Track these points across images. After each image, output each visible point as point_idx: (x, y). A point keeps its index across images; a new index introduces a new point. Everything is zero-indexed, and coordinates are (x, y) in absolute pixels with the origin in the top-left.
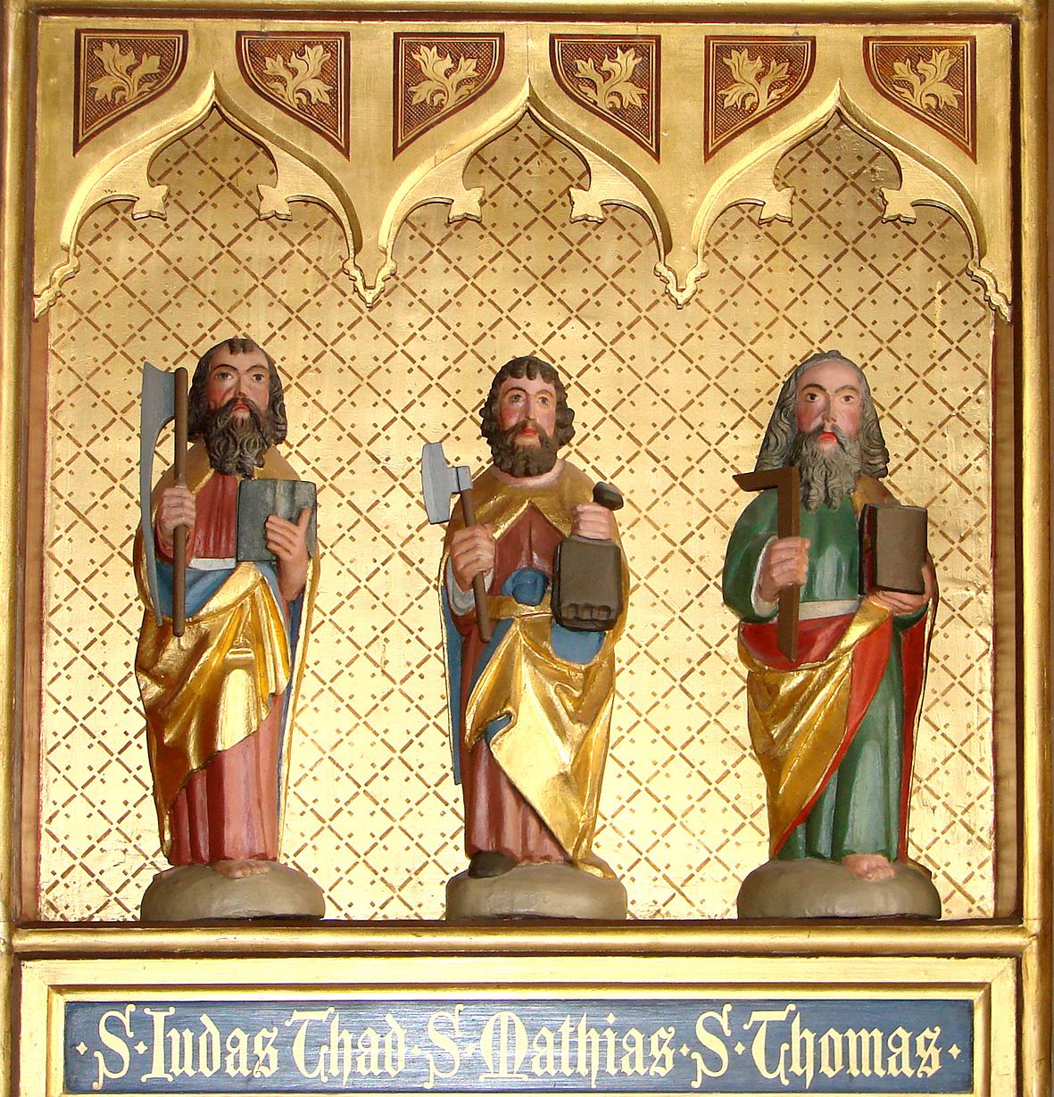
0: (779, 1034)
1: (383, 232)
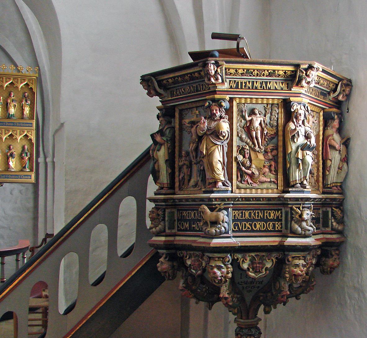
0: (23, 176)
1: (19, 139)
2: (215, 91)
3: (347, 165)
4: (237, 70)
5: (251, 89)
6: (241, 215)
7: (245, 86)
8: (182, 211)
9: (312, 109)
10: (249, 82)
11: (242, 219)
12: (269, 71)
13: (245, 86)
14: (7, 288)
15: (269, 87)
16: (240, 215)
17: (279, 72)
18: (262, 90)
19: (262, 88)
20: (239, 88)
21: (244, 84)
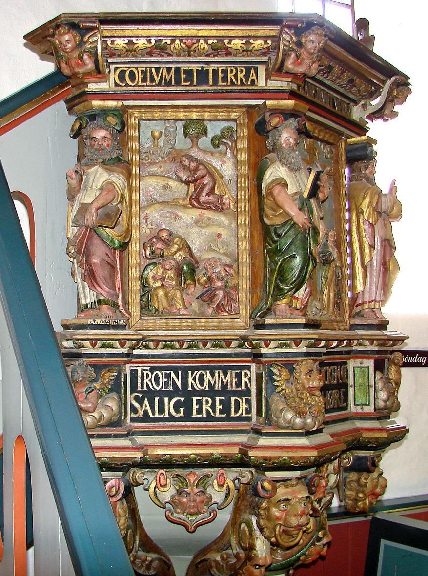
2: (84, 93)
3: (99, 287)
4: (251, 41)
5: (211, 86)
6: (197, 407)
7: (225, 79)
8: (331, 385)
9: (319, 134)
10: (169, 70)
11: (162, 416)
12: (210, 42)
13: (225, 79)
14: (355, 516)
15: (168, 80)
16: (219, 407)
17: (233, 42)
18: (227, 86)
19: (147, 81)
20: (211, 83)
21: (220, 75)
